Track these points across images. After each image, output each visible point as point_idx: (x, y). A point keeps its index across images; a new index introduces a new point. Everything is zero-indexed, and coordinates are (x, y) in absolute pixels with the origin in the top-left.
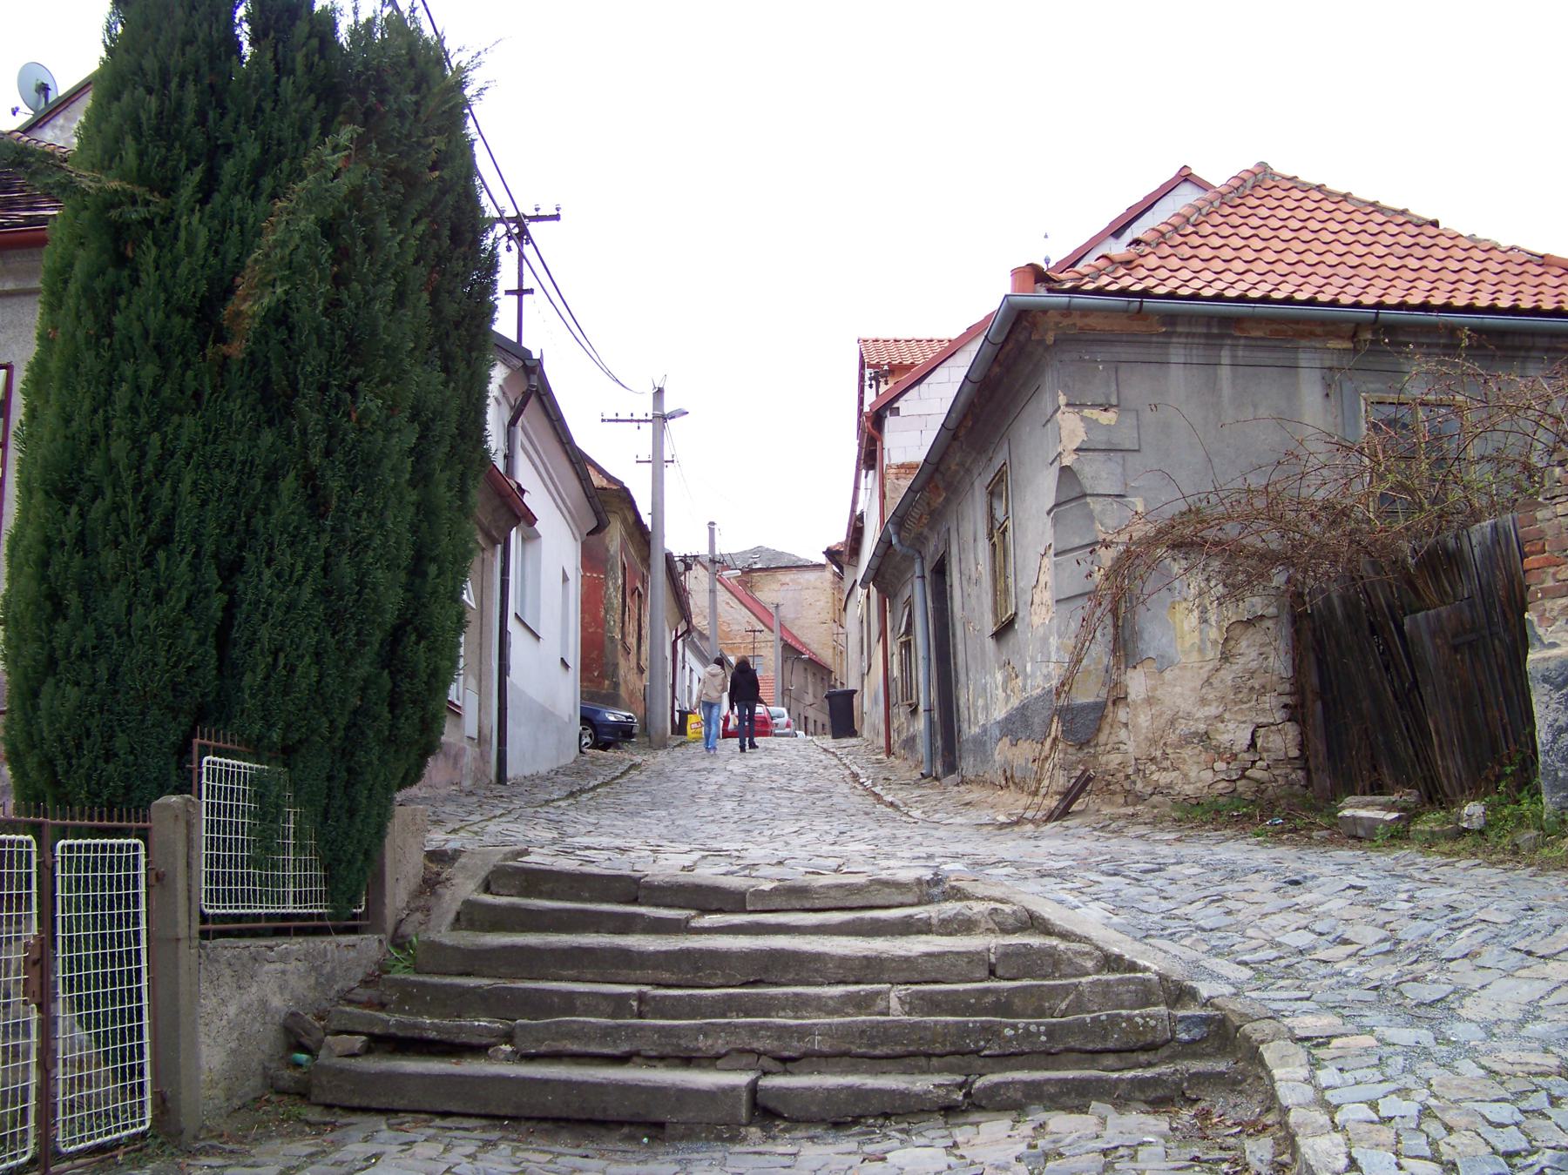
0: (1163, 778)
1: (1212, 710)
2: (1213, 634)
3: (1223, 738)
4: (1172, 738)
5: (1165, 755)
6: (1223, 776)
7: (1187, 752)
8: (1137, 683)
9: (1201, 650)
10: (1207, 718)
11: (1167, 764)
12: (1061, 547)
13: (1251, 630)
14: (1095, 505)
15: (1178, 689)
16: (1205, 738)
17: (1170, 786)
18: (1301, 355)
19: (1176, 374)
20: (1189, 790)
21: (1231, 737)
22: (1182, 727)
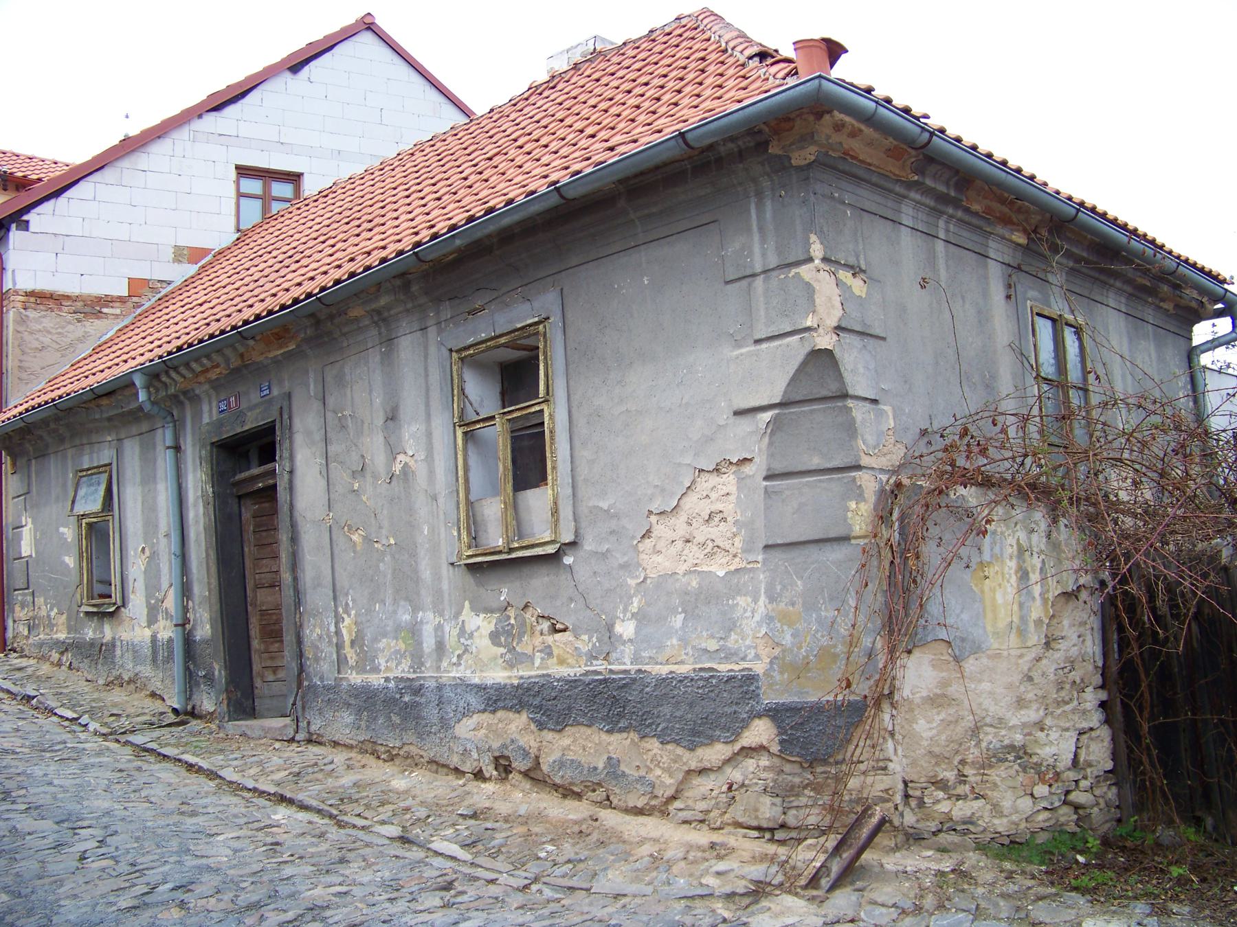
0: (960, 810)
1: (1032, 714)
2: (1036, 611)
3: (1045, 753)
4: (973, 754)
5: (962, 778)
6: (1045, 804)
7: (998, 774)
8: (918, 675)
9: (1022, 633)
10: (1024, 725)
11: (961, 790)
12: (779, 467)
13: (1071, 605)
14: (859, 412)
15: (986, 686)
16: (1020, 753)
17: (970, 821)
18: (991, 243)
19: (907, 240)
20: (1001, 825)
21: (1054, 750)
22: (990, 738)
